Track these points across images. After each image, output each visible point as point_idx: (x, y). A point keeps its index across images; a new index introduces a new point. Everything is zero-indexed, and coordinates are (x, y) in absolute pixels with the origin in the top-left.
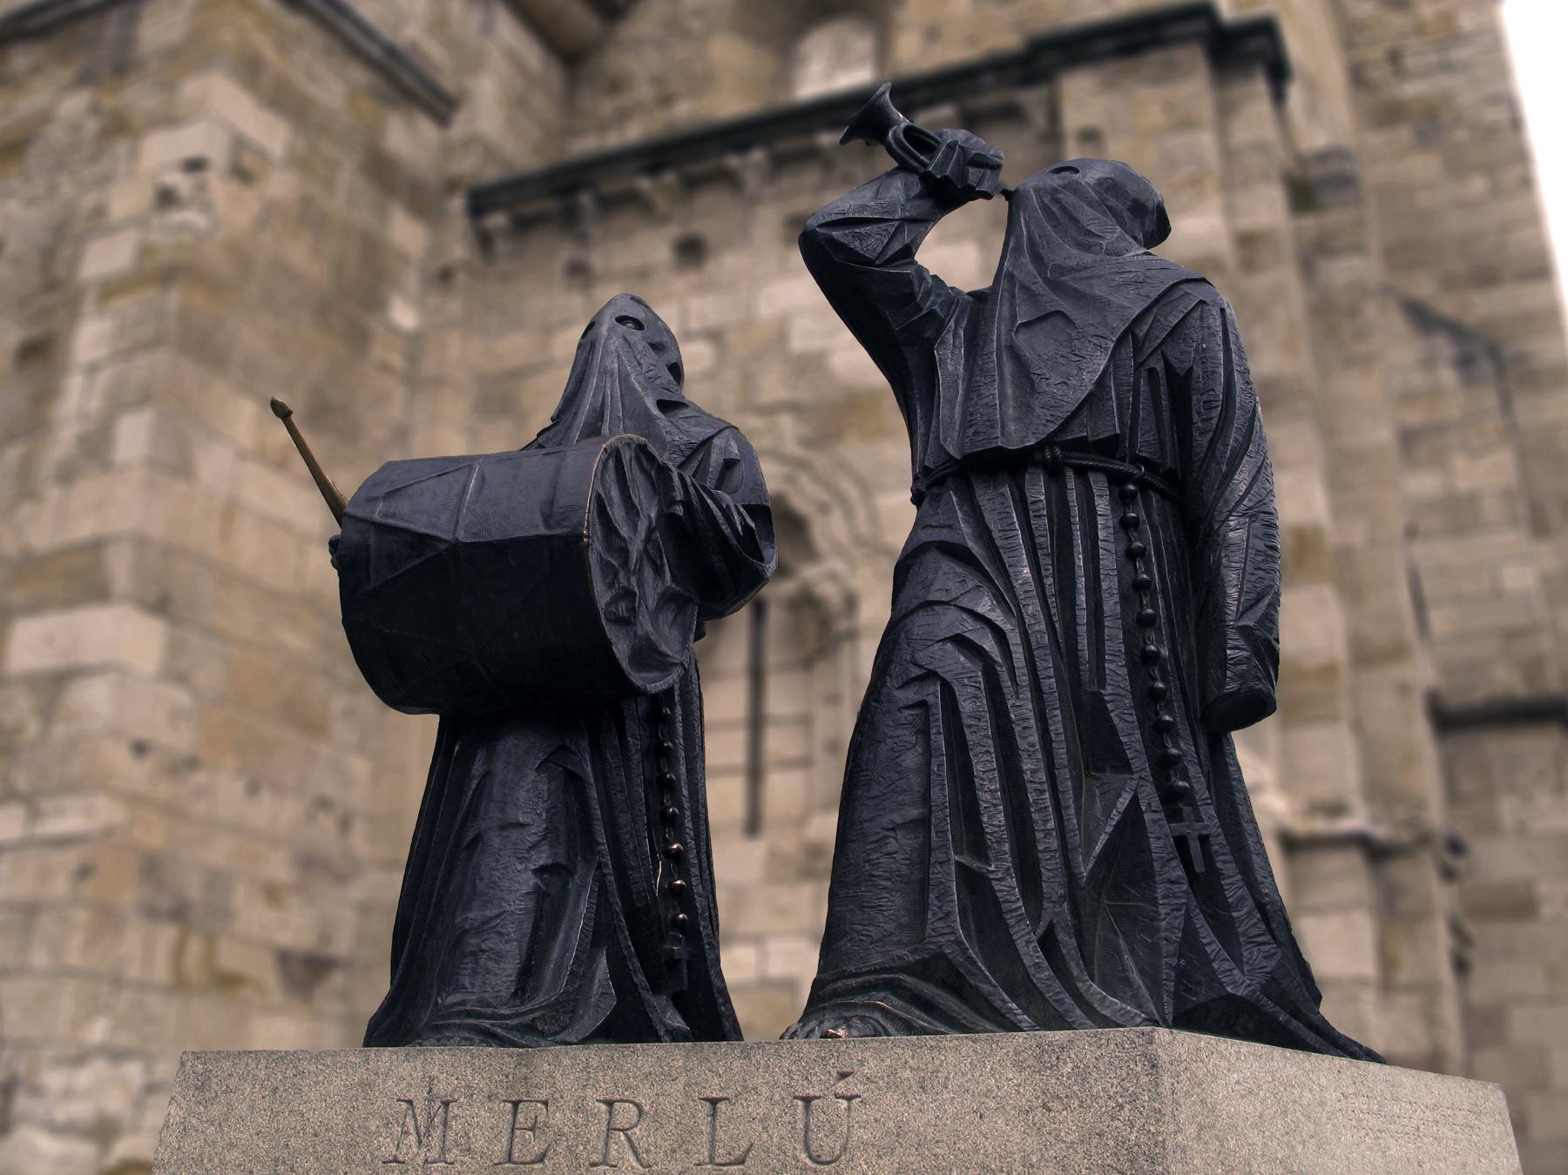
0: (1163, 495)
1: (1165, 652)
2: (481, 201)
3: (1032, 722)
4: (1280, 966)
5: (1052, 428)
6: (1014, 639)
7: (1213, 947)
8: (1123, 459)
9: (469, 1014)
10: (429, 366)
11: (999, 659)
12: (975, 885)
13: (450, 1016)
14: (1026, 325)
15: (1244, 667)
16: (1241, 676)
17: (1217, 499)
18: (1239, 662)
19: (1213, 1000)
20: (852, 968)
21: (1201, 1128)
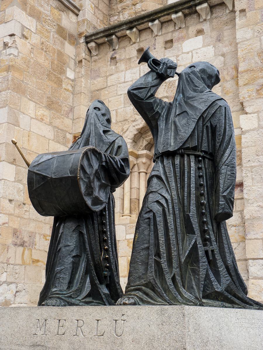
0: (209, 159)
1: (205, 202)
2: (88, 39)
3: (172, 223)
4: (230, 282)
5: (181, 144)
6: (170, 201)
7: (213, 278)
8: (198, 151)
9: (57, 294)
10: (77, 89)
11: (166, 207)
12: (158, 264)
13: (53, 294)
14: (179, 115)
15: (223, 206)
16: (223, 208)
17: (220, 161)
18: (222, 205)
19: (212, 292)
20: (132, 285)
21: (195, 330)
